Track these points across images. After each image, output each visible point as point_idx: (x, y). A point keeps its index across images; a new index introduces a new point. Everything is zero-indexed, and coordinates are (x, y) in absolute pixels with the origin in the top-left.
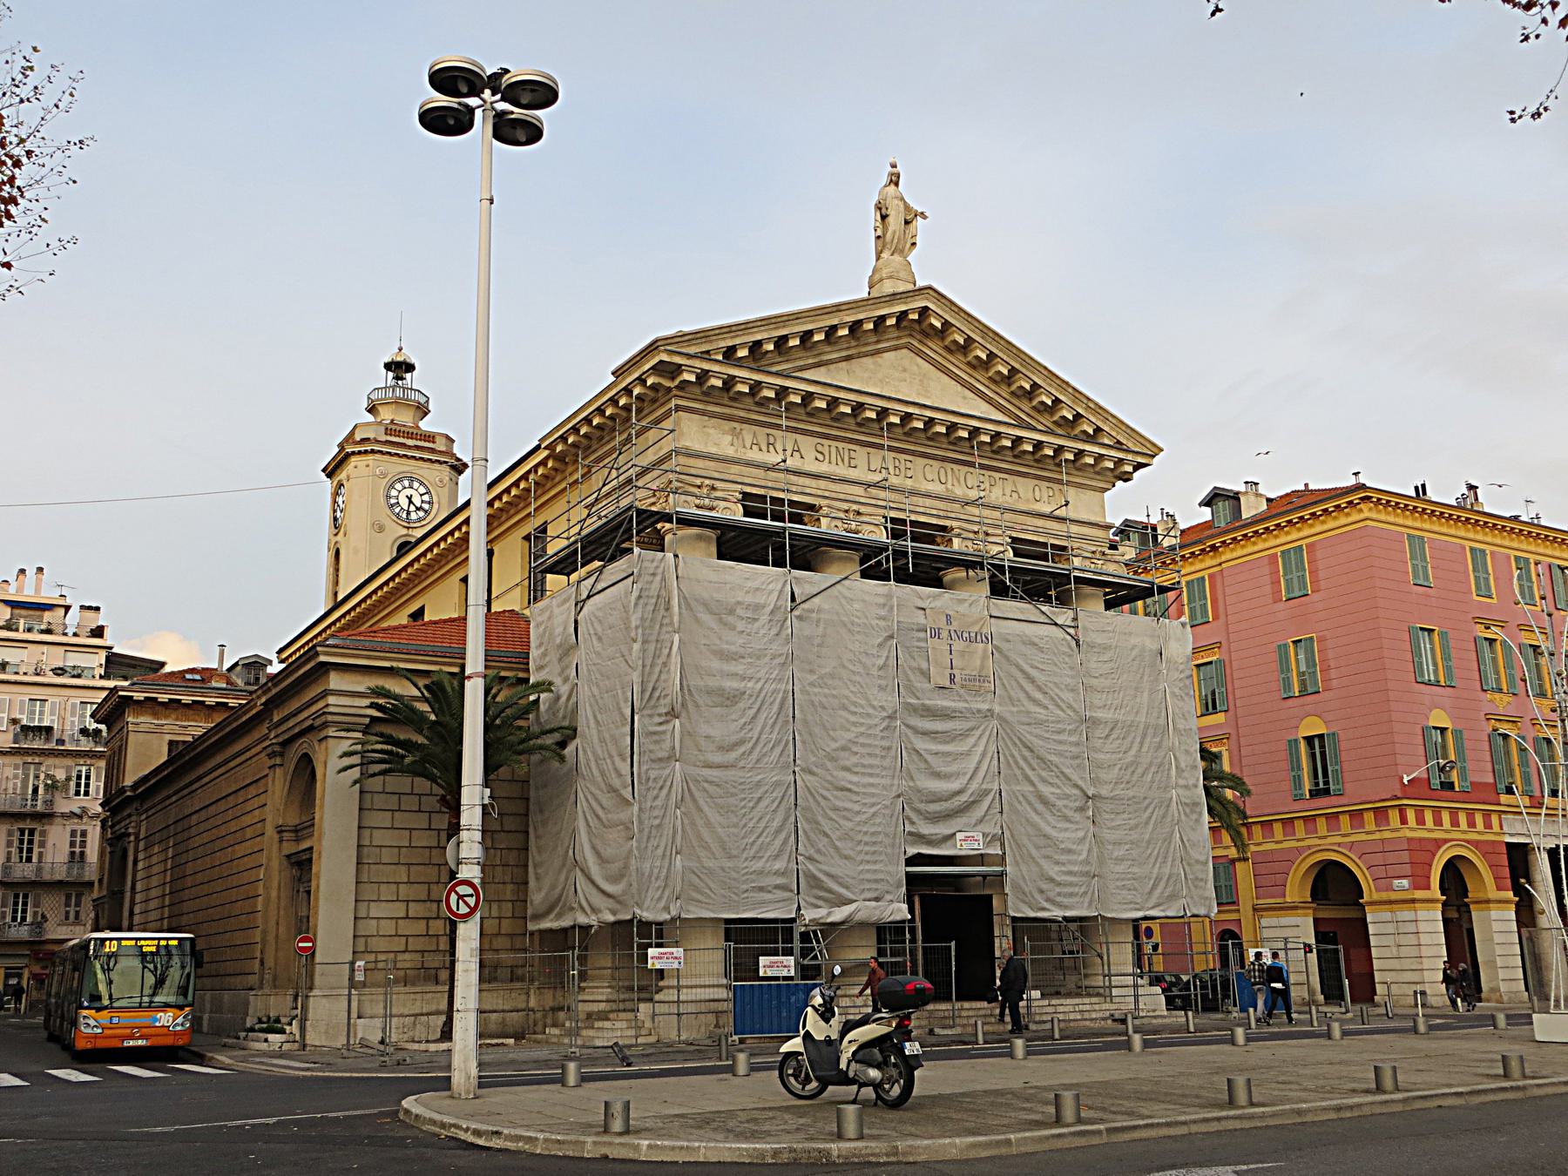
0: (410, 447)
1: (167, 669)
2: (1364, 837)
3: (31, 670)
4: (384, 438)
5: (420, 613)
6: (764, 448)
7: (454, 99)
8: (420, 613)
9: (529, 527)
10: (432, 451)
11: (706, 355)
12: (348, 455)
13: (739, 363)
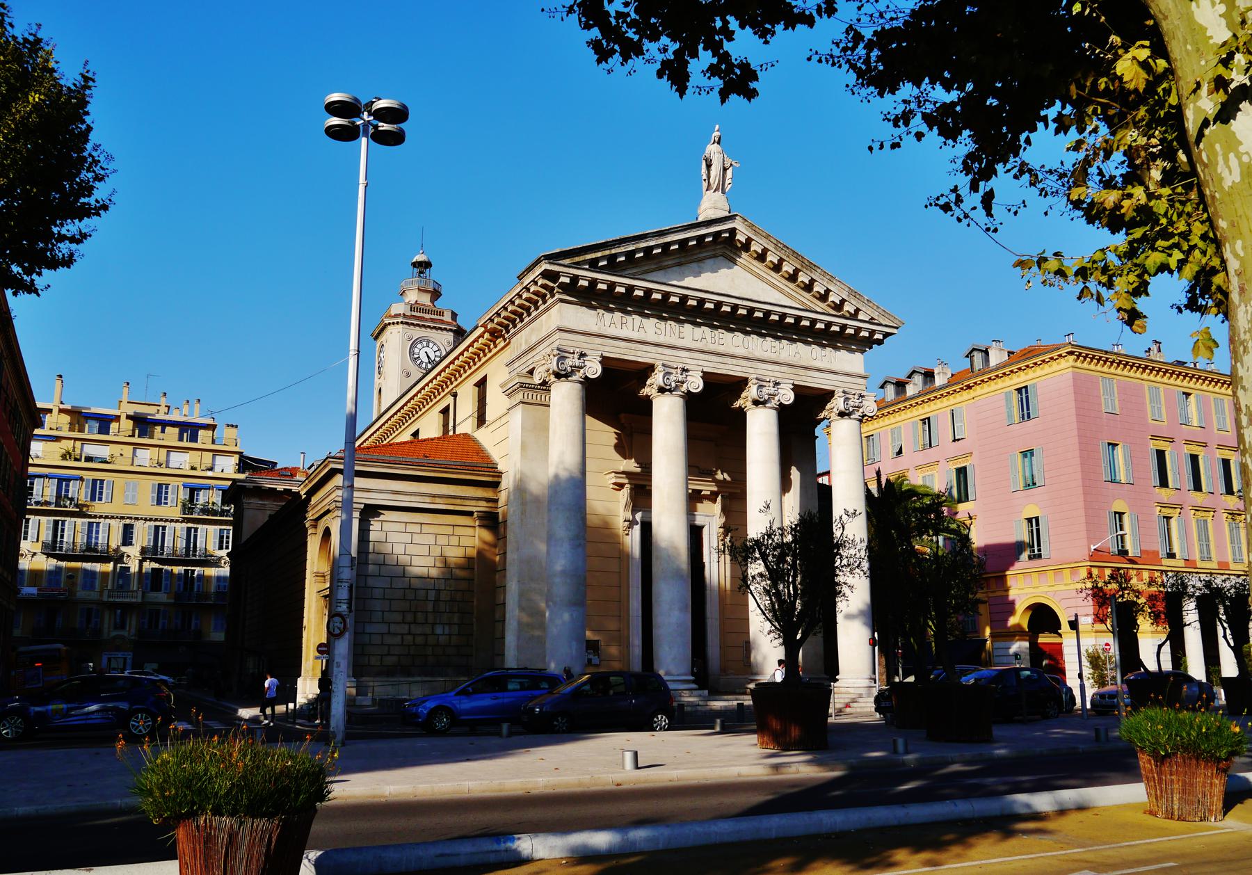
0: (426, 320)
1: (278, 467)
2: (1063, 587)
3: (188, 467)
4: (409, 313)
5: (416, 434)
6: (619, 326)
7: (347, 120)
8: (416, 434)
9: (477, 377)
10: (442, 322)
11: (577, 265)
12: (386, 325)
13: (602, 270)
